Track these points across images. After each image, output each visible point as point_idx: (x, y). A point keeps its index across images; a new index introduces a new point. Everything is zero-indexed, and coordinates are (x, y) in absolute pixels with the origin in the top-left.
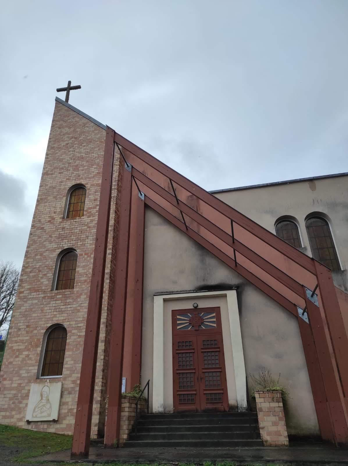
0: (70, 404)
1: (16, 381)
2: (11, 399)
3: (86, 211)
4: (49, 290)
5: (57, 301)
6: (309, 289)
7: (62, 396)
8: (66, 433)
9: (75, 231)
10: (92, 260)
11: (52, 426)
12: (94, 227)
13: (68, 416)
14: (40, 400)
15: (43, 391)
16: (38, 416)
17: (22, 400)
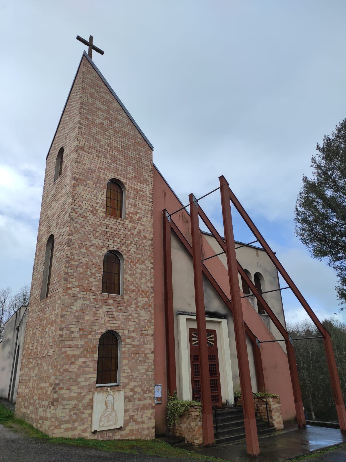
0: (131, 410)
1: (75, 391)
2: (71, 410)
5: (109, 306)
11: (117, 434)
13: (131, 422)
15: (108, 400)
16: (105, 425)
17: (84, 411)
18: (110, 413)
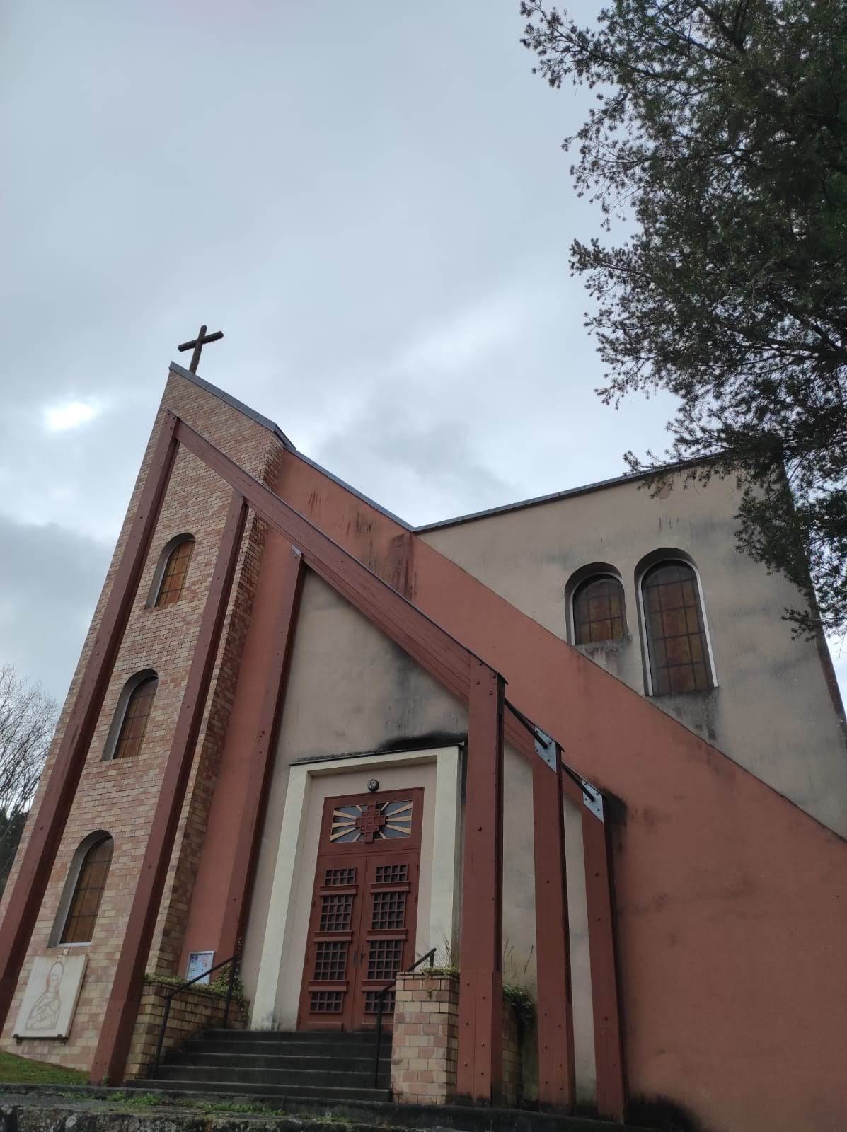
0: (95, 1002)
3: (188, 589)
4: (98, 759)
6: (541, 731)
7: (82, 986)
8: (78, 1066)
9: (162, 633)
10: (182, 694)
11: (56, 1051)
12: (196, 621)
13: (88, 1029)
14: (44, 993)
15: (53, 974)
16: (35, 1027)
18: (50, 1002)
